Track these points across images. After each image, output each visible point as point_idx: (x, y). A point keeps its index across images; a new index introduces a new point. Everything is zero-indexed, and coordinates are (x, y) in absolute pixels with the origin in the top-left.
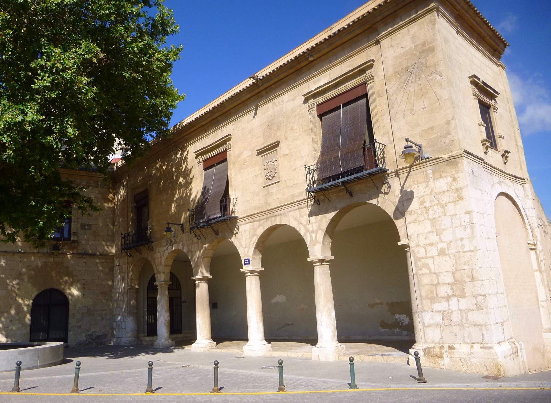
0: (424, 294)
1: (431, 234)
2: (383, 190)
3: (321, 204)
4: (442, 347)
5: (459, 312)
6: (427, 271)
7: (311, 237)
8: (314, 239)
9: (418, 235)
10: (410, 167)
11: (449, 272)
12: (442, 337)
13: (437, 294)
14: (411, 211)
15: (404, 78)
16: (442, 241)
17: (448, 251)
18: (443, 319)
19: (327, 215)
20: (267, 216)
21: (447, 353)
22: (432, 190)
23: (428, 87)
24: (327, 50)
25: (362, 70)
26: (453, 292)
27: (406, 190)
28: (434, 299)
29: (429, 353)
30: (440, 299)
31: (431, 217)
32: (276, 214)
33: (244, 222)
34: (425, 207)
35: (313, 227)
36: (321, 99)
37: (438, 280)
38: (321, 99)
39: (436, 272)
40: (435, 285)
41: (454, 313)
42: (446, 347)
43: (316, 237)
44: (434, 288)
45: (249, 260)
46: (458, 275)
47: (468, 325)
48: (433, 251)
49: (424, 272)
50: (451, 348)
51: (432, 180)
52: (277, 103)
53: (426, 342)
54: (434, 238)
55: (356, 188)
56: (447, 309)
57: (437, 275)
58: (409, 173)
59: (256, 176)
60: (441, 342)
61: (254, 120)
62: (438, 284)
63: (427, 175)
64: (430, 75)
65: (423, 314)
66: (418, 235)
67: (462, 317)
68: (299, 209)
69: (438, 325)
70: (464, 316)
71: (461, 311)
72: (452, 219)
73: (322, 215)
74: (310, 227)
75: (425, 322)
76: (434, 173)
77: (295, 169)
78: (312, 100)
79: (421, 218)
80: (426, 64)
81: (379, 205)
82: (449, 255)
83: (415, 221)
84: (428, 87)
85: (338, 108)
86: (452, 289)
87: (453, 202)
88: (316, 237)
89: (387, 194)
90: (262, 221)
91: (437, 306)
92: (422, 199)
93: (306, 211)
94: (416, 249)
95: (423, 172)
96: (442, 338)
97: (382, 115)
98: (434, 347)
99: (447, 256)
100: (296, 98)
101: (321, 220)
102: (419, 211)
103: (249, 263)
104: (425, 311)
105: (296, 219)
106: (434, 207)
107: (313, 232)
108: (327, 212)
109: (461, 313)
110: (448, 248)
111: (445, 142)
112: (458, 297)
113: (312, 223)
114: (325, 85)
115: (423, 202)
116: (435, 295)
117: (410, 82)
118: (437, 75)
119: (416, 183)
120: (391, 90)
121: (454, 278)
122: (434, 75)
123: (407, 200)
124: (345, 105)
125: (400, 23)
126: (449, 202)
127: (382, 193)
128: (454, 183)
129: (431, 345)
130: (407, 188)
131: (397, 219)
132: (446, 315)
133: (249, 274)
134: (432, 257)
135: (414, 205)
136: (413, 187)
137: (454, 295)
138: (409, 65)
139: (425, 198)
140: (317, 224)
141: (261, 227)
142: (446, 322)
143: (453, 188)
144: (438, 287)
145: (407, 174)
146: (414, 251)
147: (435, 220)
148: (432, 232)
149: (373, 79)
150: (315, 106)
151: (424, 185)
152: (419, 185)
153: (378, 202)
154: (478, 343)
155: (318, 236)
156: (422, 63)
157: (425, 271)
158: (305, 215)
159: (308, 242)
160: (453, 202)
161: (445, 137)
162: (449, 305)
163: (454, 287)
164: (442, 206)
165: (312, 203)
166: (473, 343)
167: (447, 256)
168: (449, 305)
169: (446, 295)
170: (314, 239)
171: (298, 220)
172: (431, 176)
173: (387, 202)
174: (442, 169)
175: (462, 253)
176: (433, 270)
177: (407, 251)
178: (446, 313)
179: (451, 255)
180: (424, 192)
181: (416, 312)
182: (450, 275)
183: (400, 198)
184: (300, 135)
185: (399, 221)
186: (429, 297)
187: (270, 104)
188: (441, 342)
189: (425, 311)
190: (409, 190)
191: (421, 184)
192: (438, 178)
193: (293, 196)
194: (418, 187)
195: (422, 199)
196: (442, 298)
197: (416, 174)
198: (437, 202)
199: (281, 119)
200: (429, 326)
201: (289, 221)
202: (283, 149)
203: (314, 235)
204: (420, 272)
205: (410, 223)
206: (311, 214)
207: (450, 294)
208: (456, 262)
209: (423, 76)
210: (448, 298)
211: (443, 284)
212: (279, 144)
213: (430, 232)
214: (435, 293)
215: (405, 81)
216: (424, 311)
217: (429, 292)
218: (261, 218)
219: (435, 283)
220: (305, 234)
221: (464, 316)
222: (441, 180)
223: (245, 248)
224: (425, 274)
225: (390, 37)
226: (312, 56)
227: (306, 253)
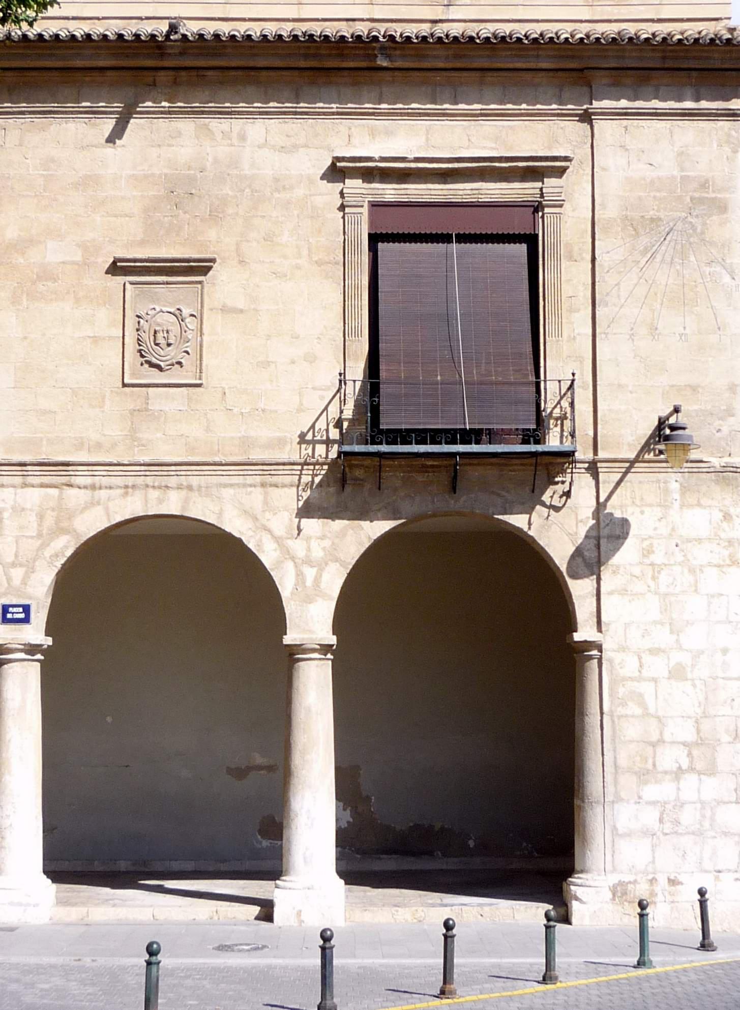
0: (623, 762)
1: (659, 626)
2: (546, 498)
3: (348, 489)
4: (653, 881)
5: (699, 806)
6: (638, 711)
7: (300, 575)
8: (309, 582)
9: (627, 625)
10: (632, 463)
11: (689, 717)
12: (654, 857)
13: (654, 765)
14: (618, 567)
15: (644, 241)
16: (681, 648)
17: (692, 671)
18: (661, 821)
19: (365, 524)
20: (130, 481)
21: (666, 894)
22: (673, 529)
23: (700, 288)
24: (441, 65)
25: (534, 170)
26: (691, 762)
27: (612, 514)
28: (645, 775)
29: (625, 893)
30: (659, 776)
31: (663, 589)
32: (173, 481)
33: (18, 480)
34: (652, 564)
35: (309, 549)
36: (390, 192)
37: (661, 734)
38: (390, 192)
39: (660, 714)
40: (654, 745)
41: (688, 808)
42: (662, 880)
43: (317, 580)
44: (650, 749)
45: (26, 609)
46: (706, 726)
47: (713, 834)
48: (657, 667)
49: (629, 712)
50: (673, 882)
51: (676, 505)
52: (219, 136)
53: (614, 870)
54: (663, 637)
55: (474, 473)
56: (672, 798)
57: (660, 721)
58: (625, 474)
59: (96, 339)
60: (650, 869)
61: (109, 150)
62: (661, 741)
63: (667, 491)
64: (709, 264)
65: (616, 806)
66: (627, 625)
67: (703, 816)
68: (263, 485)
69: (648, 833)
70: (708, 813)
71: (702, 803)
72: (709, 604)
73: (346, 522)
74: (298, 547)
75: (618, 826)
76: (684, 490)
77: (266, 364)
78: (358, 182)
79: (639, 587)
80: (703, 233)
81: (531, 533)
82: (693, 680)
83: (623, 592)
84: (700, 288)
85: (445, 238)
86: (690, 754)
87: (719, 566)
88: (317, 580)
89: (557, 509)
90: (103, 493)
91: (651, 792)
92: (646, 543)
93: (289, 499)
94: (617, 657)
95: (658, 481)
96: (653, 862)
97: (571, 310)
98: (635, 882)
99: (689, 682)
100: (295, 147)
101: (342, 534)
102: (637, 571)
103: (26, 620)
104: (622, 800)
105: (247, 513)
106: (674, 568)
107: (308, 562)
108: (363, 514)
109: (703, 808)
110: (693, 666)
111: (719, 431)
112: (699, 773)
113: (308, 539)
114: (417, 160)
115: (649, 551)
116: (650, 766)
117: (659, 258)
118: (724, 271)
119: (638, 502)
120: (606, 257)
121: (698, 731)
122: (718, 269)
123: (609, 537)
124: (463, 238)
125: (414, 106)
126: (710, 564)
127: (543, 504)
128: (725, 524)
129: (627, 878)
130: (615, 508)
131: (575, 576)
132: (668, 812)
133: (22, 655)
134: (655, 680)
135: (626, 556)
136: (630, 510)
137: (691, 769)
138: (662, 215)
139: (655, 542)
140: (327, 543)
141: (98, 511)
142: (668, 827)
143: (723, 535)
144: (659, 750)
145: (620, 475)
146: (611, 661)
147: (673, 599)
148: (662, 624)
149: (561, 206)
150: (366, 204)
151: (658, 512)
152: (644, 508)
153: (530, 524)
154: (729, 871)
155: (326, 577)
156: (693, 227)
157: (633, 709)
158: (286, 509)
159: (286, 586)
160: (719, 566)
161: (721, 419)
162: (678, 789)
163: (695, 752)
164: (692, 571)
165: (317, 480)
166: (719, 872)
167: (689, 682)
168: (678, 789)
169: (675, 767)
170: (309, 582)
171: (255, 519)
172: (677, 496)
173: (555, 528)
174: (704, 489)
175: (721, 681)
176: (652, 710)
177: (591, 658)
178: (669, 807)
179: (697, 682)
180: (655, 529)
181: (598, 802)
182: (690, 723)
183: (591, 528)
184: (298, 267)
185: (579, 582)
186: (637, 769)
187: (186, 126)
188: (650, 869)
189: (622, 800)
190: (618, 514)
191: (651, 505)
192: (691, 506)
193: (246, 442)
194: (642, 512)
195: (646, 543)
196: (666, 772)
197: (640, 482)
198: (682, 558)
199: (227, 190)
200: (628, 835)
201: (220, 514)
202: (222, 284)
203: (310, 573)
204: (620, 711)
205: (610, 593)
206: (307, 511)
207: (685, 766)
208: (706, 699)
209: (692, 258)
210: (678, 773)
211: (673, 743)
212: (210, 268)
213: (655, 623)
214: (650, 761)
215: (646, 250)
216: (618, 799)
217: (638, 758)
218: (105, 481)
219: (655, 737)
220: (279, 564)
221: (708, 813)
222: (697, 511)
223: (14, 565)
224: (633, 716)
225: (625, 123)
226: (389, 57)
227: (278, 621)
